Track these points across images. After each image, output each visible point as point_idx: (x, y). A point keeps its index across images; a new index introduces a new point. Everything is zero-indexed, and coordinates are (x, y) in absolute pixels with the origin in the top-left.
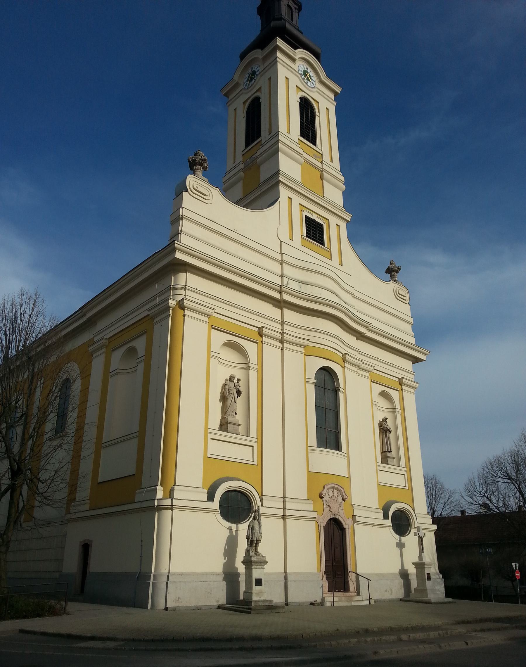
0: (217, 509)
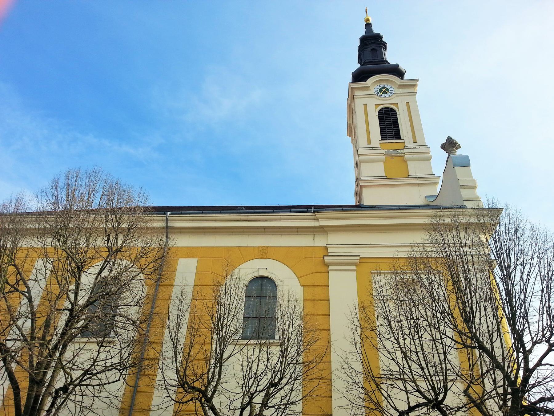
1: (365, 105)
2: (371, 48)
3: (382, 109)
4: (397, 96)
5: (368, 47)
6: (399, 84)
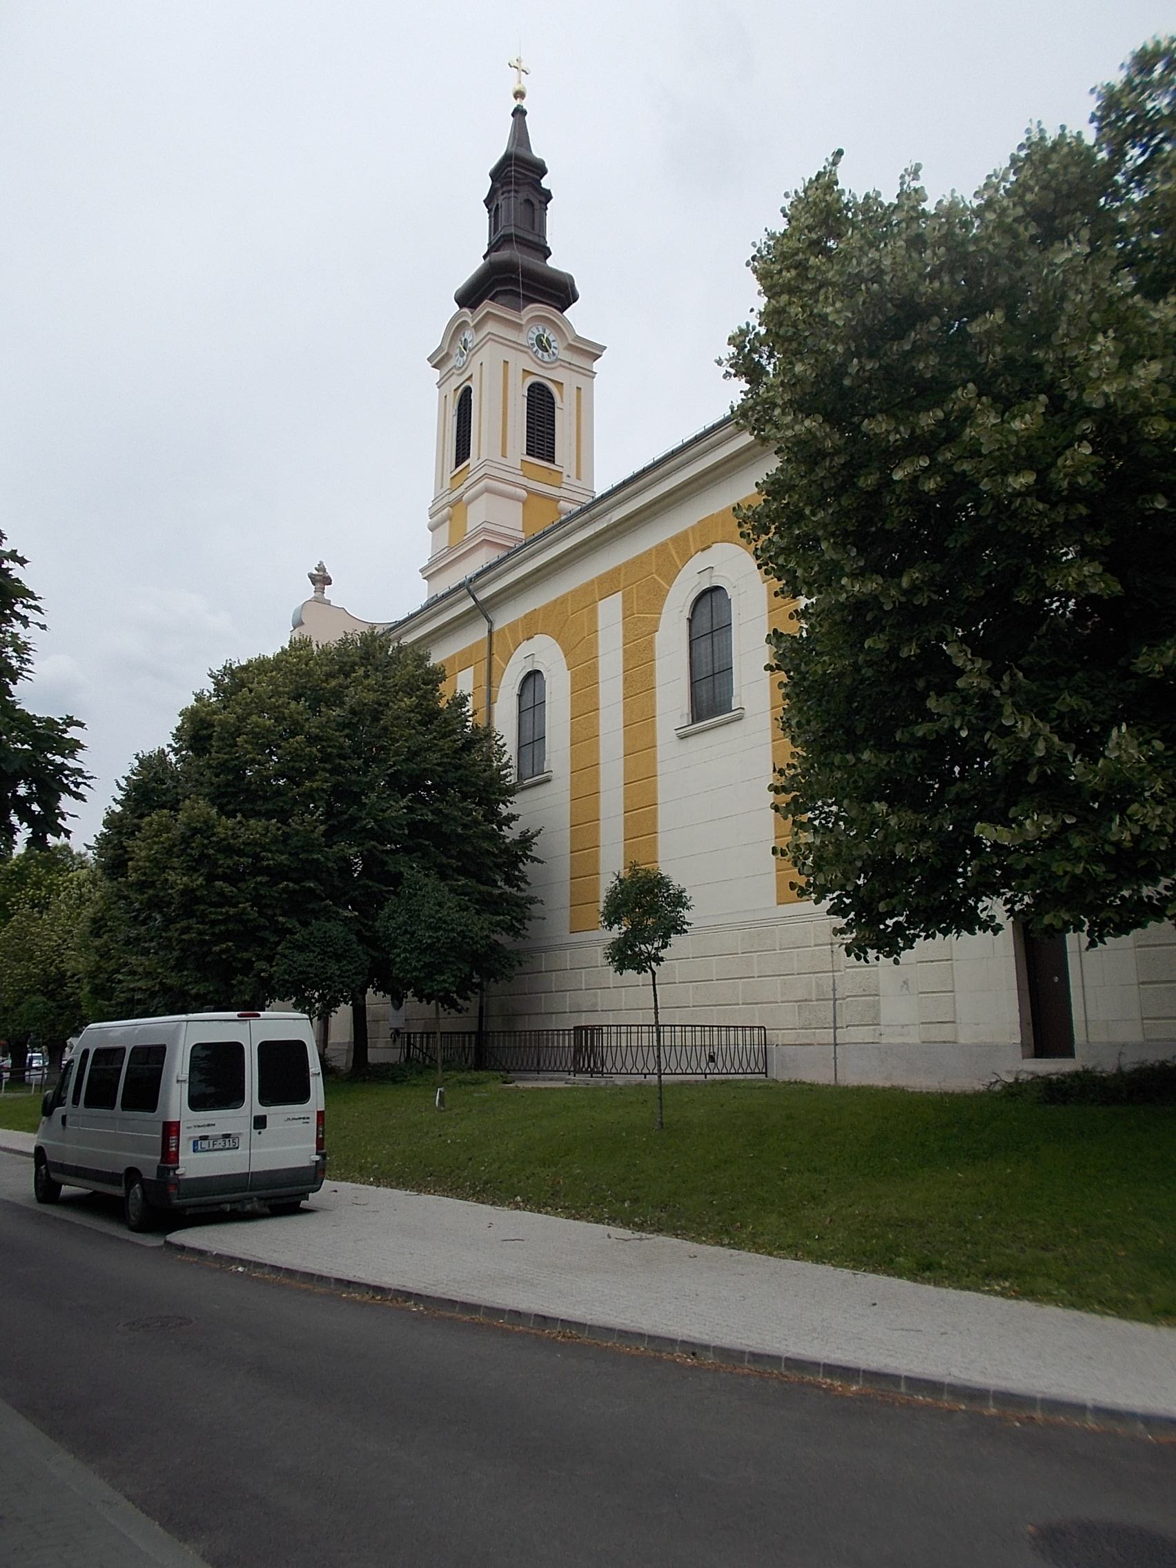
4: (561, 365)
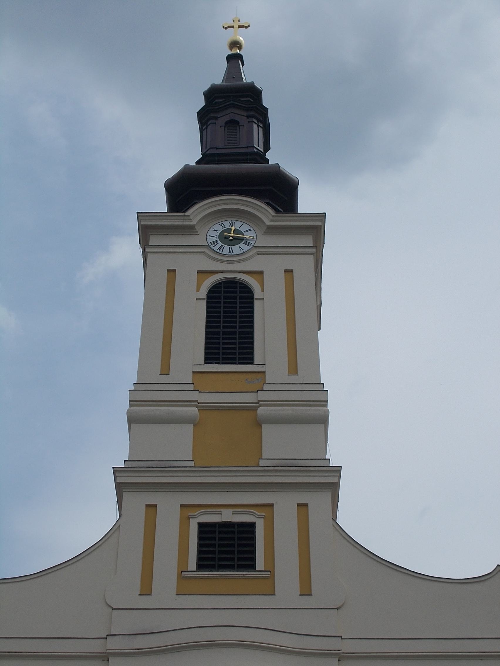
0: (258, 367)
1: (172, 272)
2: (226, 118)
3: (220, 283)
4: (258, 253)
5: (219, 115)
6: (268, 223)
